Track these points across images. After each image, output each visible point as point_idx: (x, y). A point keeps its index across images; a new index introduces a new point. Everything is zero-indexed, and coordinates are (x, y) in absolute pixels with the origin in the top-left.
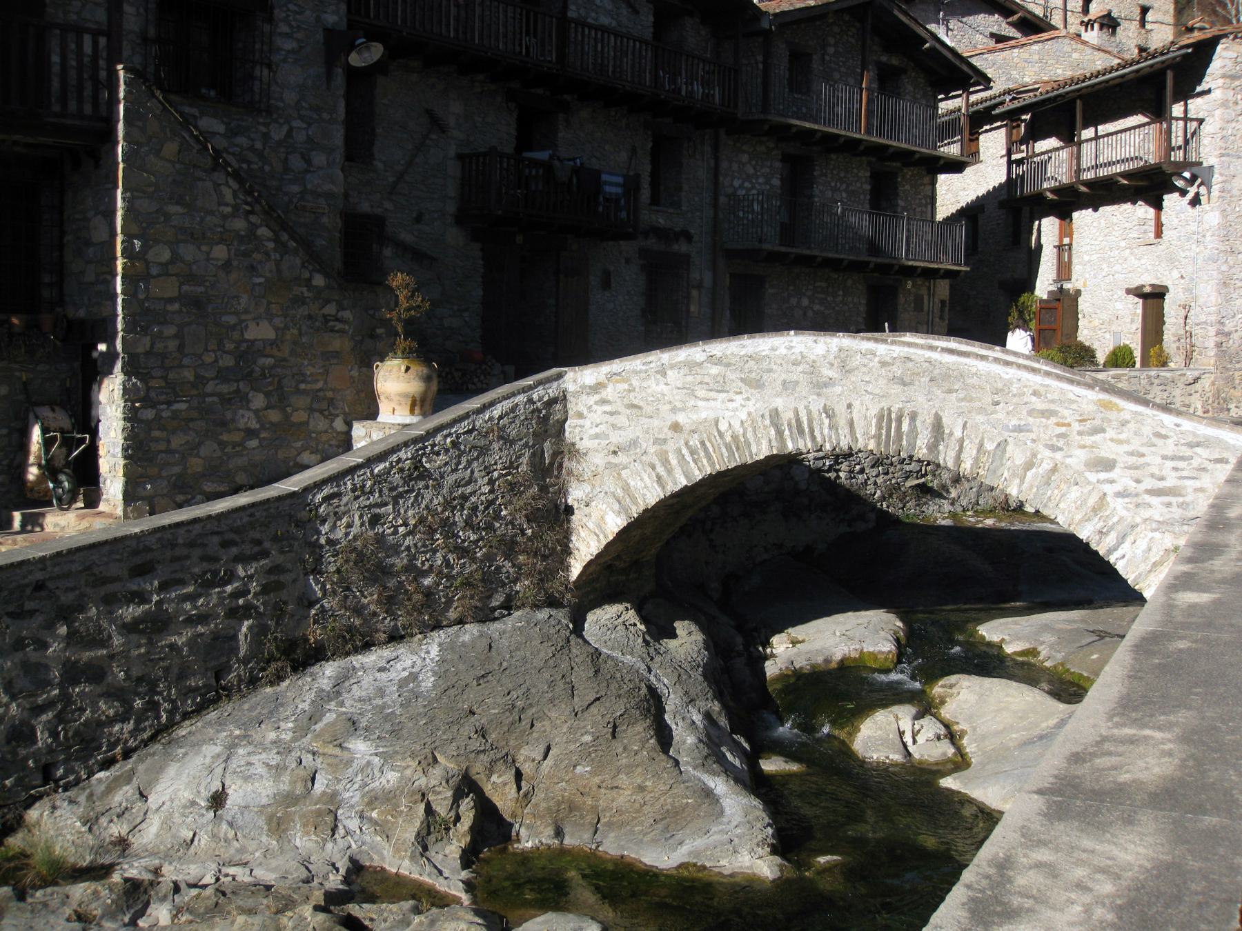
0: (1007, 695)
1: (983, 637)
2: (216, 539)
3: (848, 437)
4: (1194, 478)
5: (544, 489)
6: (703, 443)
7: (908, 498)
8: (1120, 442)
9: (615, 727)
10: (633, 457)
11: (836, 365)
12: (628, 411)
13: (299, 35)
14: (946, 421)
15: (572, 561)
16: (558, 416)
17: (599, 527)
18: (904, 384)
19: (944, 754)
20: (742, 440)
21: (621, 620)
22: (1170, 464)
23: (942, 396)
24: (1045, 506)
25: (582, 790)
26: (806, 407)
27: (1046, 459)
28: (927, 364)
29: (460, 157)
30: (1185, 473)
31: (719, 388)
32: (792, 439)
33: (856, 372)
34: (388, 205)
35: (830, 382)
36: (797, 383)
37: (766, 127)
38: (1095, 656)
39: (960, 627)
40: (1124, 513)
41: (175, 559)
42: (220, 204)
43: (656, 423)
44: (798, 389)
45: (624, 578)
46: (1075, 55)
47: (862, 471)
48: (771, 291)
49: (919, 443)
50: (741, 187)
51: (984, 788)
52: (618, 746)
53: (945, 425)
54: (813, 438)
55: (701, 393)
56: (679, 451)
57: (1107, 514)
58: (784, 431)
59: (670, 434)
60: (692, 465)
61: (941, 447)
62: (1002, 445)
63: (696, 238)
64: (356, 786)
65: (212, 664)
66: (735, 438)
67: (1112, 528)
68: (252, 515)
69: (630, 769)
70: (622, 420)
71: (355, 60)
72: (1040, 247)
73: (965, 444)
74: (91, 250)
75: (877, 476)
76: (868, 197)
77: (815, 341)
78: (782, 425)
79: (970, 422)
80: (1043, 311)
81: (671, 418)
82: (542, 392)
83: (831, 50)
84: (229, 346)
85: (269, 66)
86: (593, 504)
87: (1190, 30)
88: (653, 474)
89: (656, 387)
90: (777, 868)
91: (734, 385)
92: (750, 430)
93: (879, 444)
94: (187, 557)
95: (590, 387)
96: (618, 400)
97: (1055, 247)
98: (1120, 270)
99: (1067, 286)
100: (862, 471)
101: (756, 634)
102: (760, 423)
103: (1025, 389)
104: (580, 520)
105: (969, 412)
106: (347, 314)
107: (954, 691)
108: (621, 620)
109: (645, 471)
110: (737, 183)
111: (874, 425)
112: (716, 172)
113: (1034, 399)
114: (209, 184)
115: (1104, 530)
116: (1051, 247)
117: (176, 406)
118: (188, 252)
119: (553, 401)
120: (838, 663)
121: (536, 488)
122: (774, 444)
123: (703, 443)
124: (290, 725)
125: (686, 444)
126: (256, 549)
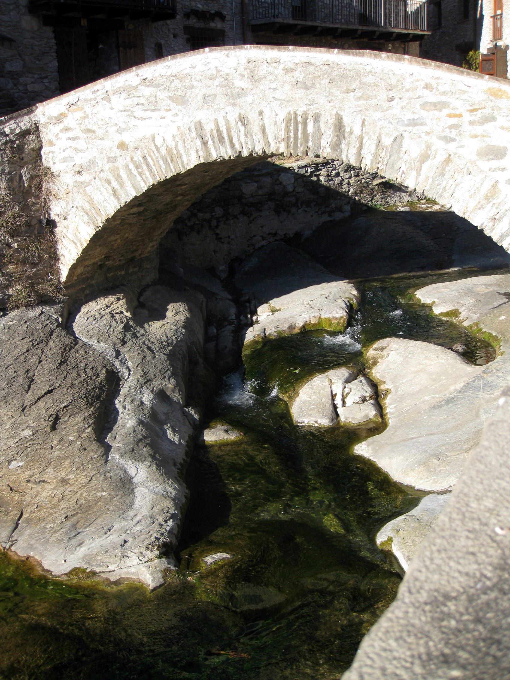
0: (426, 358)
1: (419, 300)
3: (262, 142)
5: (25, 208)
6: (144, 158)
7: (375, 193)
9: (57, 418)
10: (94, 175)
11: (246, 75)
12: (85, 135)
14: (346, 121)
15: (61, 266)
16: (32, 146)
17: (75, 235)
18: (307, 88)
19: (367, 416)
20: (175, 152)
21: (109, 310)
23: (341, 96)
24: (441, 196)
25: (12, 485)
26: (225, 118)
28: (326, 67)
31: (153, 108)
32: (215, 148)
33: (264, 81)
35: (243, 92)
36: (215, 95)
38: (503, 318)
39: (403, 292)
43: (107, 144)
44: (216, 102)
45: (123, 273)
47: (338, 175)
49: (324, 143)
51: (390, 458)
52: (55, 437)
53: (346, 124)
54: (233, 146)
55: (138, 112)
56: (127, 166)
57: (499, 201)
58: (207, 141)
59: (118, 152)
60: (138, 178)
61: (343, 146)
62: (398, 139)
63: (228, 18)
66: (169, 150)
72: (482, 16)
73: (364, 141)
75: (350, 178)
77: (227, 56)
78: (206, 136)
79: (367, 119)
80: (484, 62)
81: (118, 138)
82: (13, 126)
86: (69, 217)
88: (110, 188)
90: (160, 575)
91: (164, 103)
92: (180, 142)
93: (288, 147)
95: (56, 118)
96: (77, 127)
97: (491, 17)
99: (500, 43)
100: (338, 175)
101: (248, 305)
102: (188, 136)
103: (418, 84)
104: (62, 232)
105: (367, 110)
107: (385, 353)
108: (109, 310)
109: (103, 186)
111: (283, 129)
113: (426, 92)
115: (497, 217)
116: (489, 17)
119: (25, 133)
120: (301, 329)
121: (17, 209)
122: (201, 153)
123: (144, 158)
125: (132, 159)
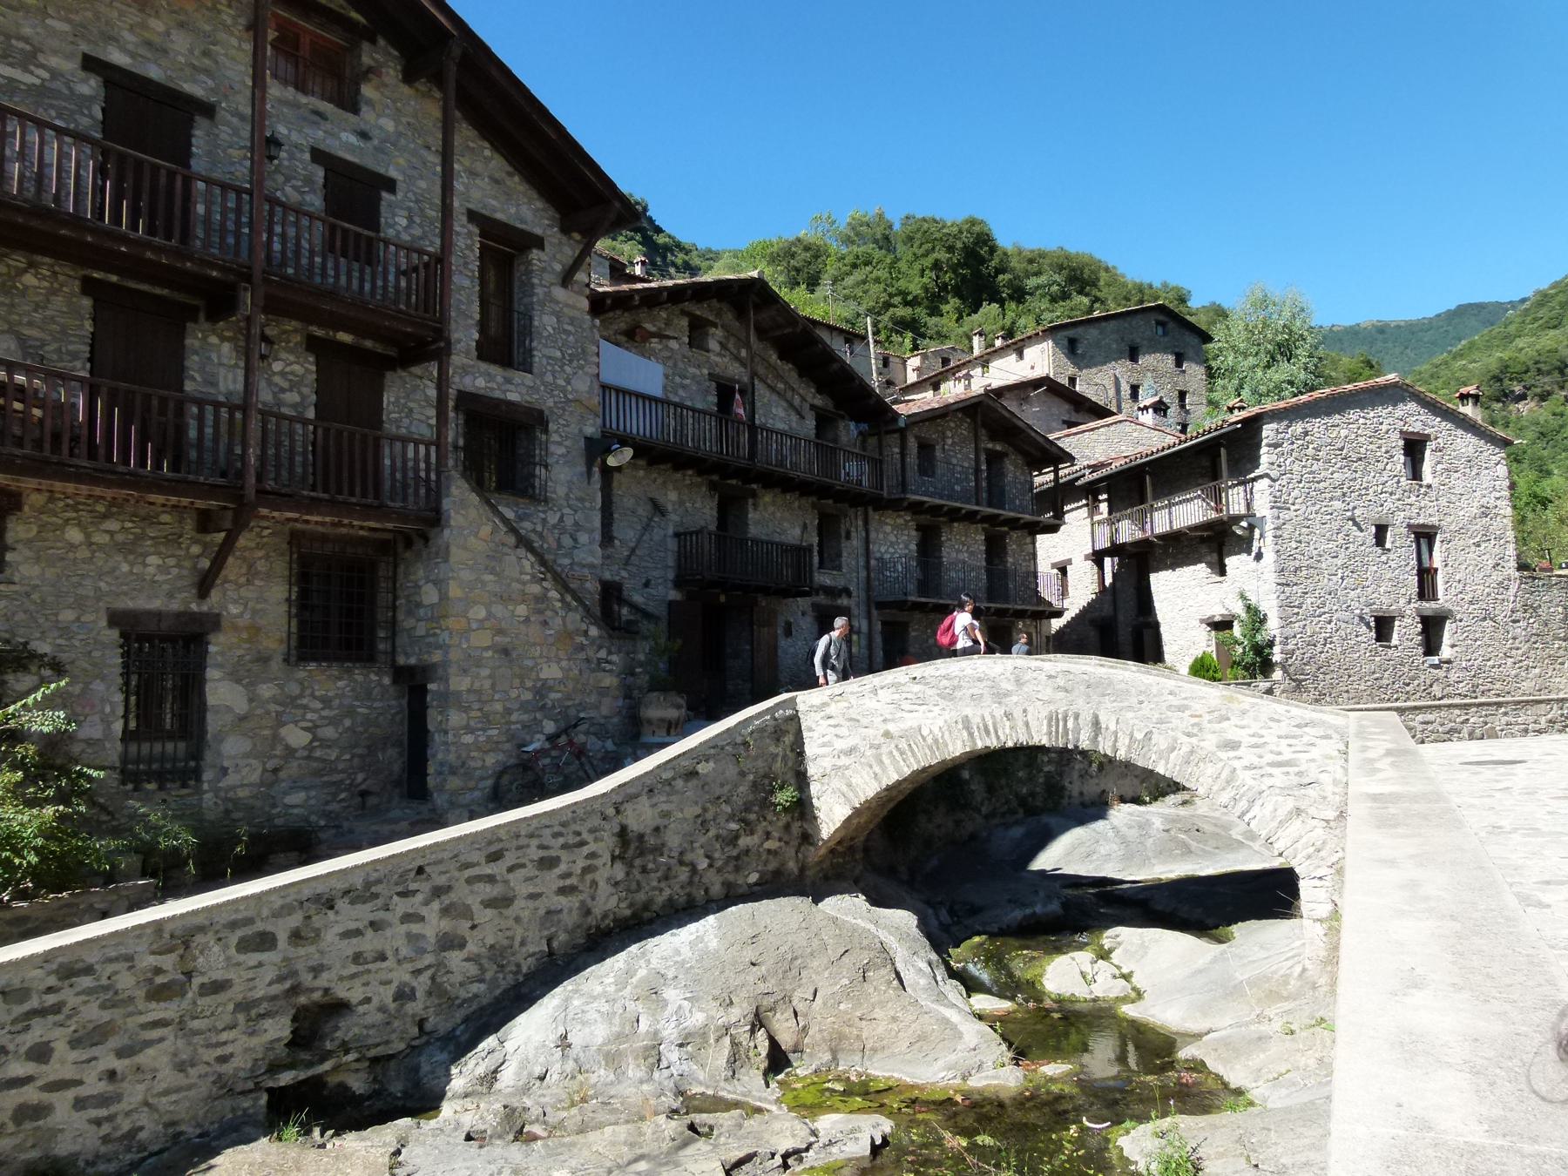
2: (548, 832)
8: (1243, 727)
13: (567, 443)
14: (1102, 718)
18: (1067, 691)
22: (1284, 742)
27: (1186, 744)
29: (677, 535)
30: (1298, 749)
34: (624, 574)
35: (1007, 694)
37: (905, 504)
40: (1252, 782)
41: (519, 848)
42: (521, 574)
43: (870, 732)
46: (1135, 434)
48: (913, 634)
49: (1082, 737)
50: (886, 552)
54: (998, 738)
59: (882, 740)
60: (902, 763)
63: (854, 594)
64: (673, 1025)
65: (546, 933)
66: (936, 741)
67: (1243, 796)
68: (574, 812)
69: (883, 1004)
70: (843, 731)
71: (612, 461)
74: (422, 612)
83: (949, 441)
84: (529, 684)
85: (546, 467)
89: (870, 703)
94: (528, 846)
106: (614, 658)
110: (883, 549)
112: (867, 541)
114: (513, 558)
117: (490, 732)
118: (498, 610)
124: (612, 980)
126: (578, 839)
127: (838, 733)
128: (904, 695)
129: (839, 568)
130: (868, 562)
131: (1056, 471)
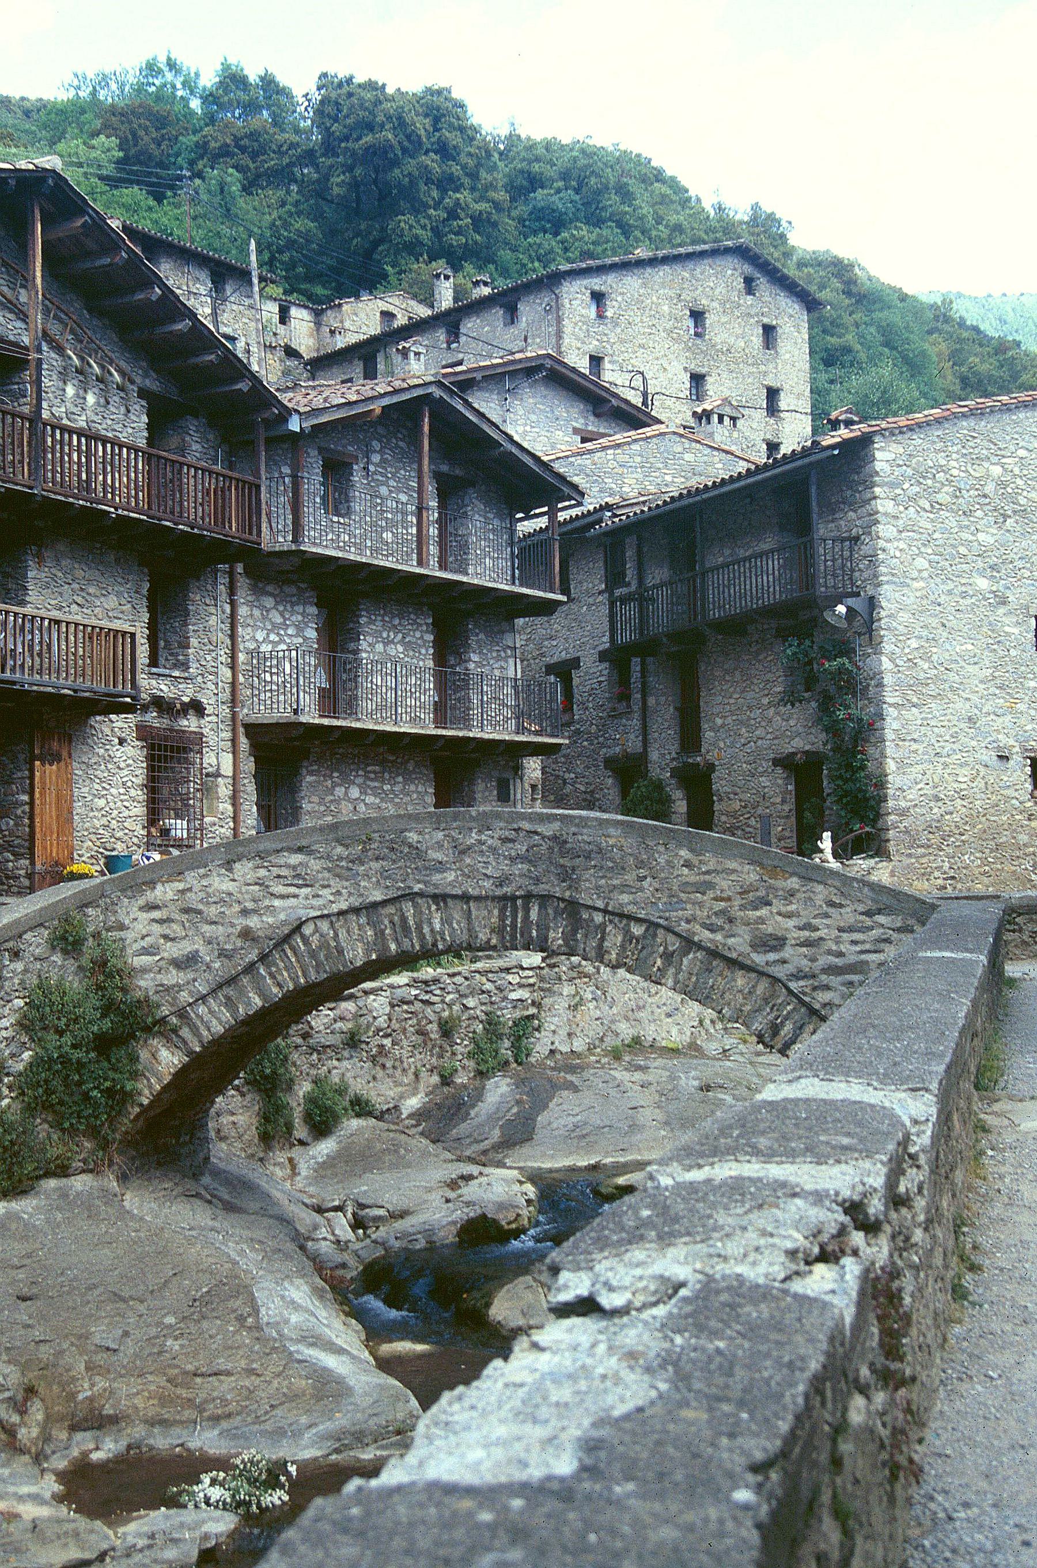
4: (875, 952)
8: (789, 916)
30: (867, 947)
46: (688, 457)
48: (309, 779)
59: (239, 943)
76: (431, 651)
81: (241, 922)
87: (835, 424)
98: (763, 735)
113: (686, 871)
127: (168, 932)
128: (275, 871)
129: (185, 666)
130: (233, 657)
131: (552, 514)
